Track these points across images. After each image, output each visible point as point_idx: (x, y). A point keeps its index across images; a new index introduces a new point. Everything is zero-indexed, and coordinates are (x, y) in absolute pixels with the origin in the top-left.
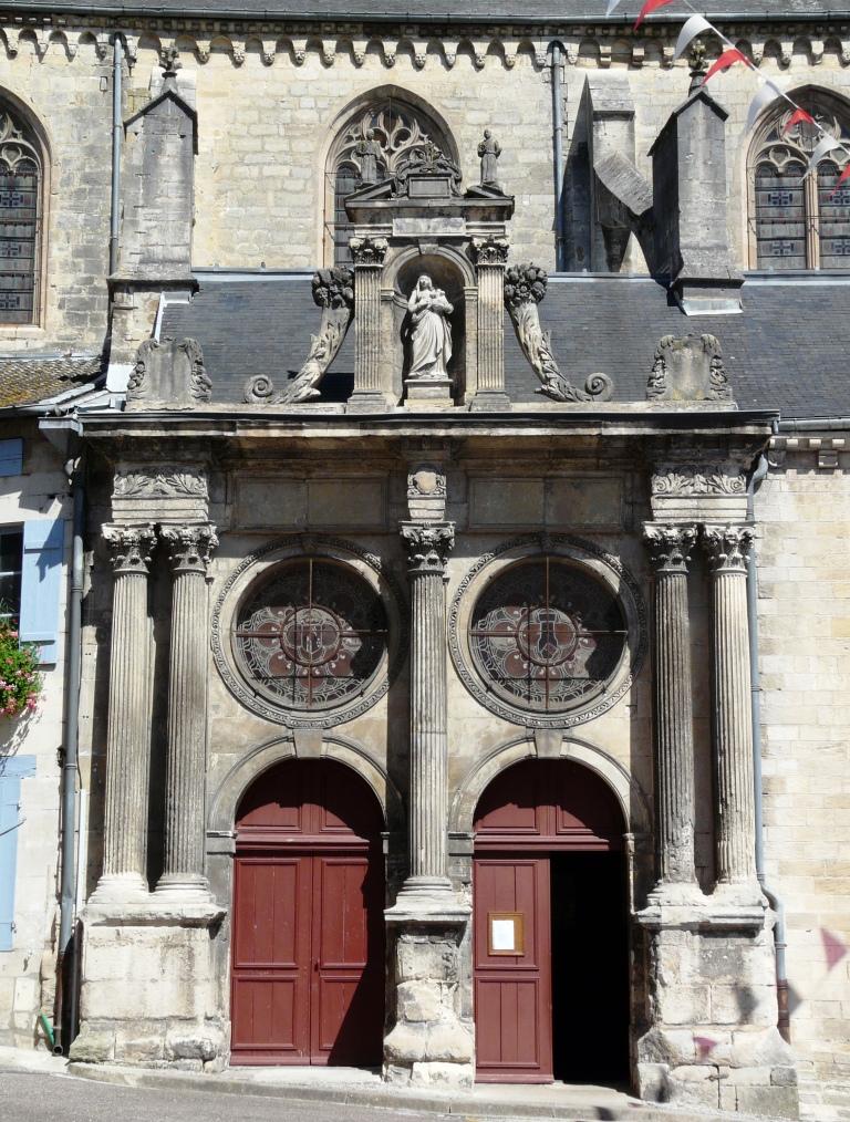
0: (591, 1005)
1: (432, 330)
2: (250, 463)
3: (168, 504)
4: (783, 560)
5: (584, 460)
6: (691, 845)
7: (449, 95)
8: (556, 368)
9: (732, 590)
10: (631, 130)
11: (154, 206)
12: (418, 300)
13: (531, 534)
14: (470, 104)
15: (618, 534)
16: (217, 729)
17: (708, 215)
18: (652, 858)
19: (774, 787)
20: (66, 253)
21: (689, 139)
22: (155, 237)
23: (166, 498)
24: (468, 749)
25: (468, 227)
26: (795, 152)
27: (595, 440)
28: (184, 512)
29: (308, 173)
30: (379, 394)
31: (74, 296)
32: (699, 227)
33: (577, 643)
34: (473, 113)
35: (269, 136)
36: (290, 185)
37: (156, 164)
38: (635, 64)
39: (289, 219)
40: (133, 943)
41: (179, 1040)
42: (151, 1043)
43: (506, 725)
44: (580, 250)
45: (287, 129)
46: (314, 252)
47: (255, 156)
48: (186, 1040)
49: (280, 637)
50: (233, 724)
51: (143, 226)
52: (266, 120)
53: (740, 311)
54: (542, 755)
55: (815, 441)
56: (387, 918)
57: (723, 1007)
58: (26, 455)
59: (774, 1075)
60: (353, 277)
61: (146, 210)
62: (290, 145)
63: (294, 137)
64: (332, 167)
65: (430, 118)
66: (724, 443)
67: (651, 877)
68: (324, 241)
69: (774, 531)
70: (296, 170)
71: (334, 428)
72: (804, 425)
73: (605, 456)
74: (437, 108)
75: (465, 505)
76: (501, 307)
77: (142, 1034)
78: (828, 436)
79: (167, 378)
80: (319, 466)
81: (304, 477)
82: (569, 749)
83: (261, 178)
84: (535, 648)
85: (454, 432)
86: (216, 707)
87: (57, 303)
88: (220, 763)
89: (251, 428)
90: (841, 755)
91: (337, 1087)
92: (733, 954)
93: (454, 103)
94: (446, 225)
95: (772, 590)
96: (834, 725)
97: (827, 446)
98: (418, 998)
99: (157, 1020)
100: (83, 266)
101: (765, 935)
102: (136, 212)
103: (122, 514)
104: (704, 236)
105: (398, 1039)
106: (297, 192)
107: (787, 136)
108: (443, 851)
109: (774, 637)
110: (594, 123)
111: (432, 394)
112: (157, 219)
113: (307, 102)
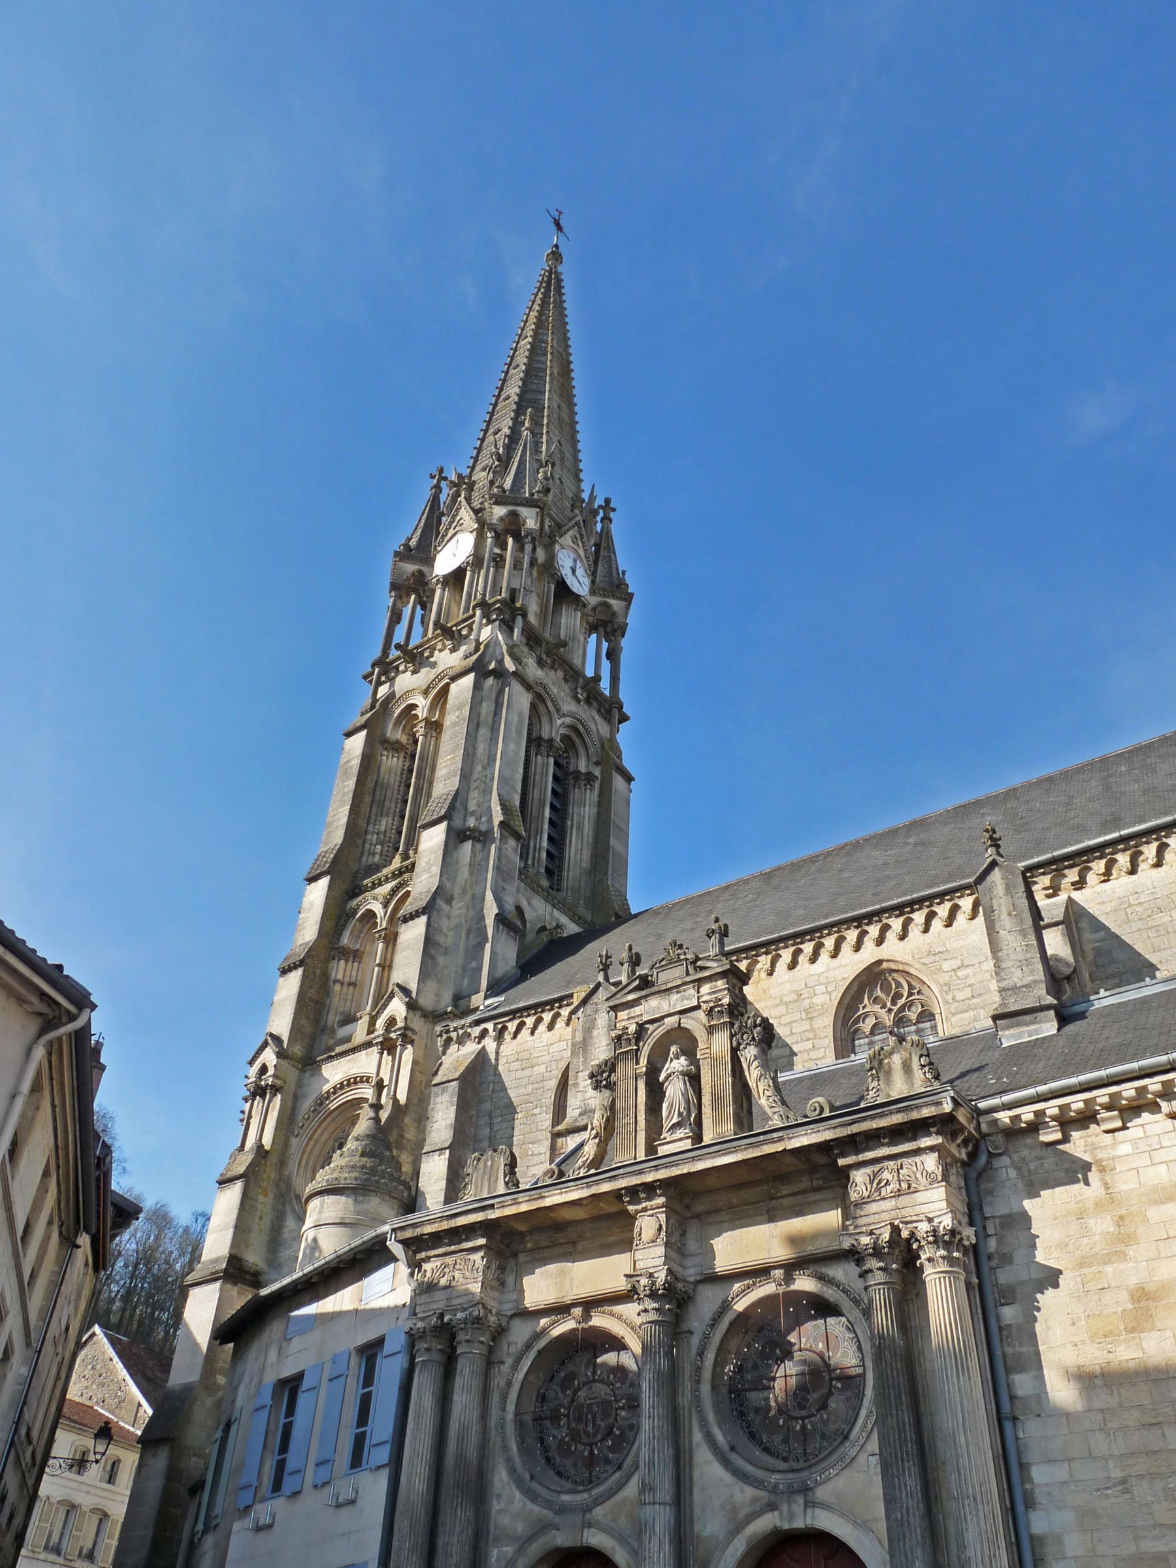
17: (1021, 957)
19: (1049, 1550)
33: (830, 1390)
43: (750, 1492)
63: (812, 1018)
79: (486, 1183)
86: (499, 1496)
88: (498, 1559)
90: (1127, 1496)
93: (931, 959)
95: (1014, 1292)
96: (1111, 1456)
113: (820, 989)
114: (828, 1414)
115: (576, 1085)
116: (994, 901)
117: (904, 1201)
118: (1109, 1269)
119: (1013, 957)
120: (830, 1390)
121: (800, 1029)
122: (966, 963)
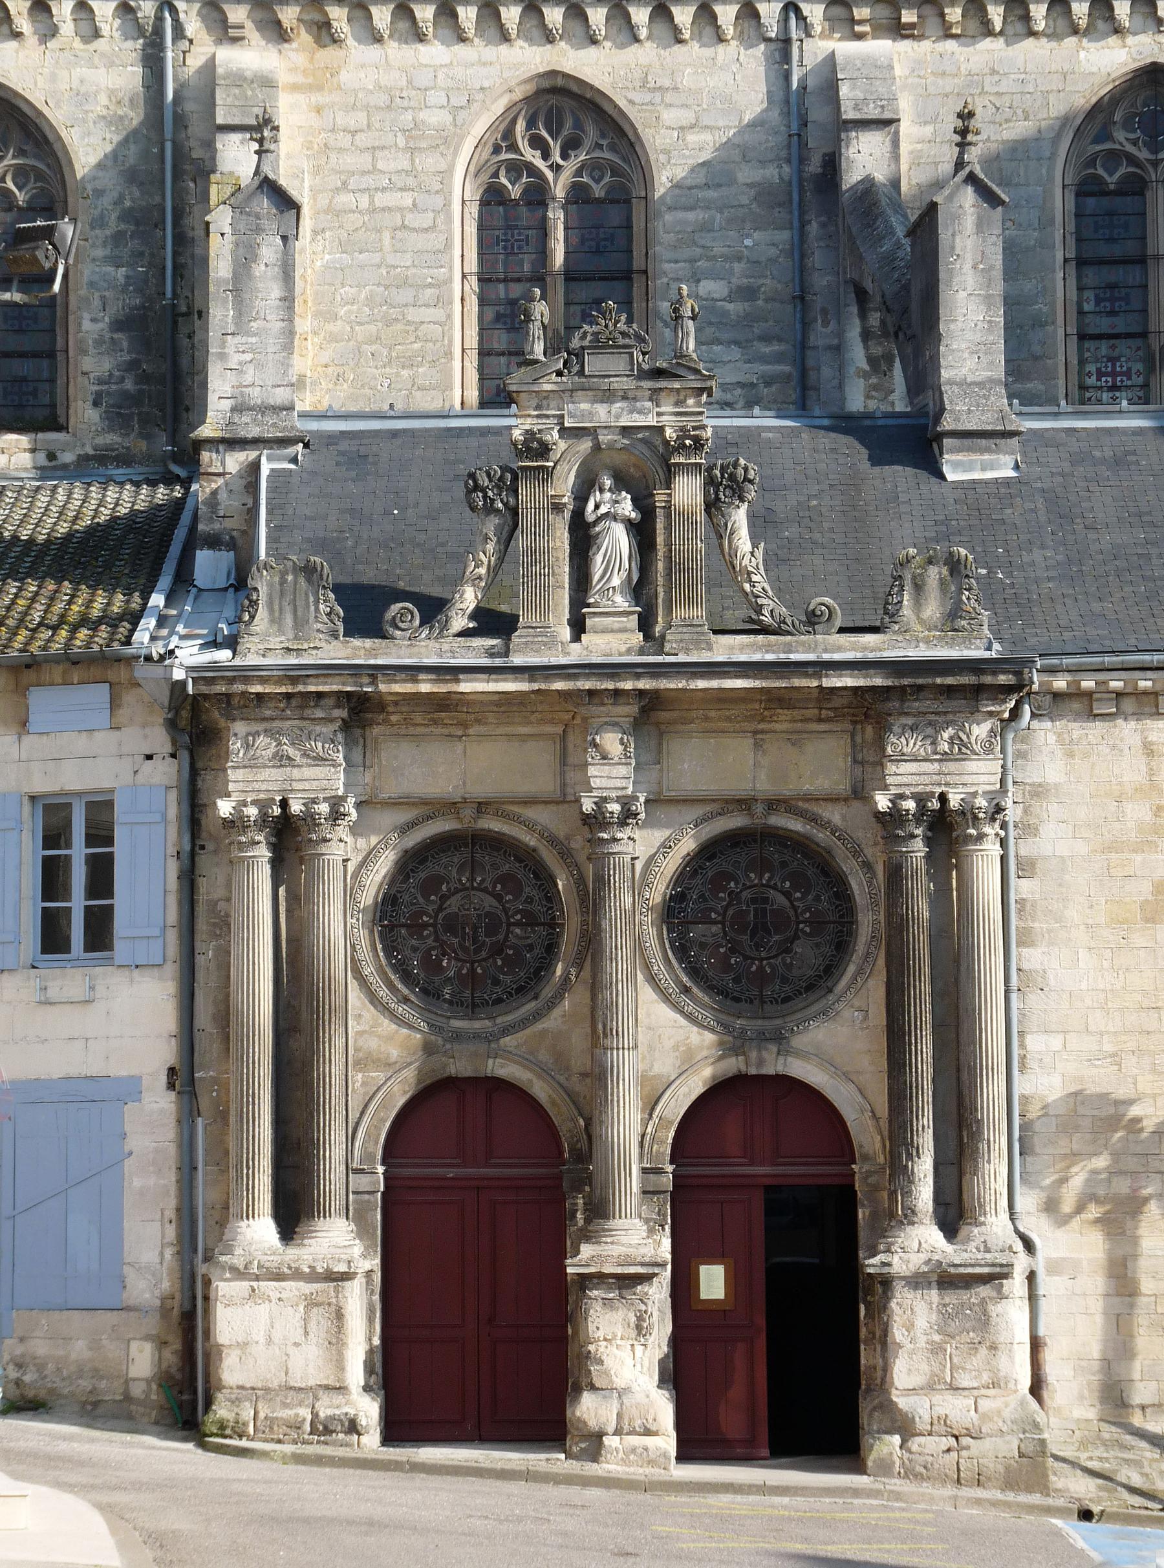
0: (792, 1374)
1: (617, 541)
2: (394, 718)
3: (296, 773)
4: (1049, 830)
5: (804, 711)
6: (930, 1180)
7: (638, 84)
8: (770, 593)
9: (985, 864)
10: (896, 143)
11: (248, 334)
12: (597, 507)
13: (738, 800)
14: (669, 97)
15: (846, 800)
16: (361, 1043)
17: (978, 337)
18: (885, 1194)
20: (100, 325)
21: (953, 235)
22: (250, 376)
23: (294, 766)
24: (664, 1066)
25: (659, 414)
26: (1132, 160)
27: (815, 694)
28: (315, 783)
29: (438, 201)
30: (547, 641)
31: (114, 387)
32: (966, 355)
33: (796, 933)
34: (673, 110)
35: (383, 148)
36: (413, 220)
37: (250, 276)
38: (899, 31)
39: (413, 271)
40: (270, 1301)
41: (329, 1412)
42: (297, 1415)
44: (824, 312)
45: (407, 139)
46: (449, 317)
47: (364, 179)
48: (337, 1412)
49: (434, 925)
50: (379, 1036)
51: (234, 360)
52: (377, 126)
53: (1013, 474)
54: (753, 1071)
55: (1088, 684)
56: (569, 1270)
57: (964, 1369)
58: (114, 704)
59: (1022, 1446)
60: (515, 478)
61: (238, 339)
62: (412, 160)
64: (473, 193)
65: (610, 116)
66: (977, 692)
67: (893, 1216)
68: (462, 299)
69: (1039, 791)
70: (421, 198)
71: (497, 681)
72: (1074, 665)
73: (828, 706)
74: (622, 103)
75: (658, 766)
76: (700, 516)
77: (285, 1405)
78: (1102, 676)
79: (288, 610)
80: (478, 721)
81: (460, 733)
82: (785, 1065)
83: (373, 210)
84: (745, 938)
85: (643, 684)
87: (91, 398)
88: (364, 1084)
89: (396, 682)
90: (1116, 1068)
91: (487, 1465)
92: (977, 1308)
94: (631, 412)
96: (1107, 1032)
97: (1103, 688)
98: (609, 1362)
99: (301, 1389)
100: (125, 344)
101: (1017, 1285)
102: (224, 342)
103: (240, 786)
104: (973, 367)
105: (589, 1409)
106: (426, 230)
107: (1120, 135)
108: (635, 1189)
109: (1036, 925)
110: (843, 136)
111: (616, 626)
112: (253, 351)
114: (792, 958)
115: (223, 356)
116: (958, 240)
117: (951, 766)
118: (1139, 858)
119: (969, 335)
120: (796, 933)
121: (392, 166)
122: (706, 121)
